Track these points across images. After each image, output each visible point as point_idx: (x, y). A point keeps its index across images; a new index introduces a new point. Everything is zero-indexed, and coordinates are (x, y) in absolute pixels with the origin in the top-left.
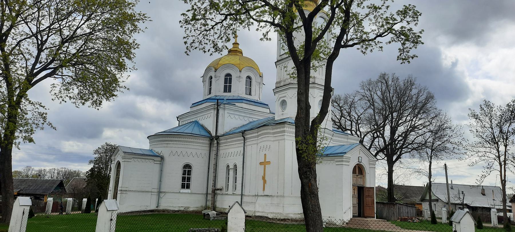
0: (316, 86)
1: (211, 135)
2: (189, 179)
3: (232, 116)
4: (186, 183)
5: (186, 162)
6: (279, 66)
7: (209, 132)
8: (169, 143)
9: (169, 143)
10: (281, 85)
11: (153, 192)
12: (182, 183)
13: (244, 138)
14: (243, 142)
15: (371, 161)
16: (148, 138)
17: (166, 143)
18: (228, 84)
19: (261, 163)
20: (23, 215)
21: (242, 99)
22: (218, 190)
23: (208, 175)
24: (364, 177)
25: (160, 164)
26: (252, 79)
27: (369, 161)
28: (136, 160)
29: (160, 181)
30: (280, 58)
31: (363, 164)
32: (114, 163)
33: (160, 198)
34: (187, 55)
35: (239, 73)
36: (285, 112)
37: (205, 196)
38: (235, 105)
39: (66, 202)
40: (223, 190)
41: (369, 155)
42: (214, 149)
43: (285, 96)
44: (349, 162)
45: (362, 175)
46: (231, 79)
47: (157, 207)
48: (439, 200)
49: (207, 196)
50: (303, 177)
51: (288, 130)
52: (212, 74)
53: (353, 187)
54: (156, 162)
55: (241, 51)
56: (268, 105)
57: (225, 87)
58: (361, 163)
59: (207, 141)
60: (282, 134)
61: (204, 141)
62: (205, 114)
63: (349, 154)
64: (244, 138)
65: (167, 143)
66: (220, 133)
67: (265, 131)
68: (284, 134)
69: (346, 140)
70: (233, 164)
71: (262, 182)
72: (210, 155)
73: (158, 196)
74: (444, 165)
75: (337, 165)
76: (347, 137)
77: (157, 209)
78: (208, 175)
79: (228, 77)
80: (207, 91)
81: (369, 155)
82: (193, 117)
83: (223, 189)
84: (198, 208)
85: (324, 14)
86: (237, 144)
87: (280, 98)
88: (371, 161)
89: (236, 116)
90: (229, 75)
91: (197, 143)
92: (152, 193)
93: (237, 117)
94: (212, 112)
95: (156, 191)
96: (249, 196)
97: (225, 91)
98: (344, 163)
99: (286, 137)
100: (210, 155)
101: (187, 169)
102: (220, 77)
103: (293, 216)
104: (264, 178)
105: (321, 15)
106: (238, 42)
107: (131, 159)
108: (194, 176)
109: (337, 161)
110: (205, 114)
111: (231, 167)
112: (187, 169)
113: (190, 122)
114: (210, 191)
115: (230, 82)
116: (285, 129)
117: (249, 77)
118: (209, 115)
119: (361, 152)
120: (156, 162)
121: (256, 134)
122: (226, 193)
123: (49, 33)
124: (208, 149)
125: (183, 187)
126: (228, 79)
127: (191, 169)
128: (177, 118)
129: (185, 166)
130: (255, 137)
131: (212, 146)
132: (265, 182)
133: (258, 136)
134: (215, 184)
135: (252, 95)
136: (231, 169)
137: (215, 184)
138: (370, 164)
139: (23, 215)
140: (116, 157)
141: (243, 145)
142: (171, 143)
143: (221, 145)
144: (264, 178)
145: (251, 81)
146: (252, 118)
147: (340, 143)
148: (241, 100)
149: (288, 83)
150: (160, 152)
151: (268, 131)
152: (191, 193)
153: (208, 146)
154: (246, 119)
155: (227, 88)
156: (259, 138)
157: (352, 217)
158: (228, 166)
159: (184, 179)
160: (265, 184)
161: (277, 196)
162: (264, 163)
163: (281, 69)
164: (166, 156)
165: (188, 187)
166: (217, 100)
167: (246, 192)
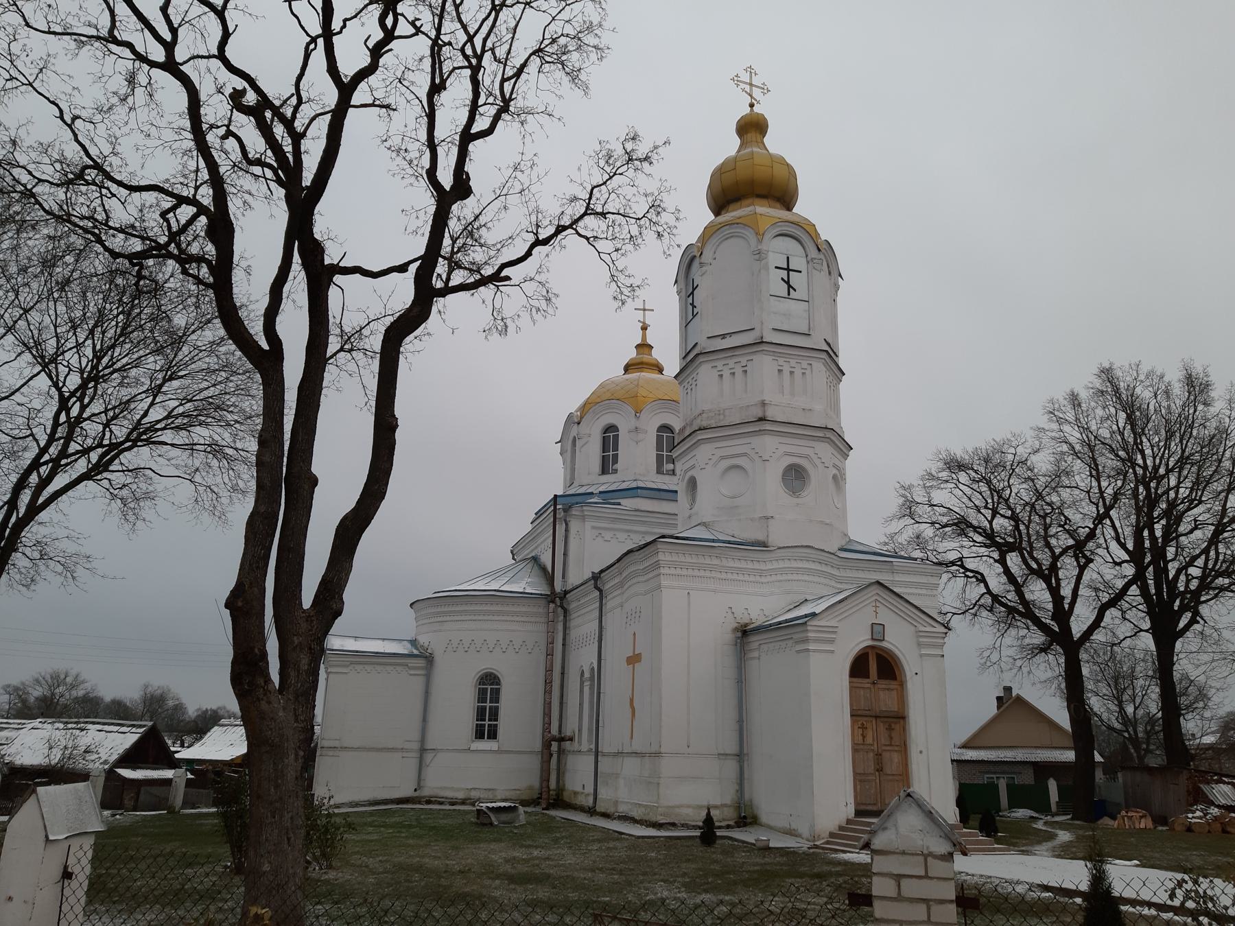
0: (768, 426)
2: (494, 714)
3: (608, 535)
4: (486, 726)
5: (484, 667)
11: (407, 751)
15: (921, 634)
24: (902, 684)
28: (359, 667)
31: (891, 643)
41: (914, 616)
43: (693, 467)
44: (832, 641)
45: (867, 680)
46: (616, 438)
47: (415, 790)
53: (854, 718)
54: (412, 672)
58: (884, 642)
63: (829, 617)
64: (601, 591)
68: (655, 573)
75: (798, 652)
76: (888, 567)
77: (417, 794)
81: (914, 616)
84: (518, 792)
85: (787, 224)
88: (921, 634)
89: (619, 535)
90: (611, 429)
101: (489, 685)
102: (590, 435)
105: (780, 229)
106: (649, 341)
108: (506, 705)
112: (489, 685)
116: (661, 556)
123: (1083, 427)
125: (479, 734)
126: (610, 437)
129: (482, 679)
138: (919, 645)
142: (448, 618)
143: (574, 616)
152: (499, 752)
158: (583, 671)
159: (481, 714)
165: (493, 735)
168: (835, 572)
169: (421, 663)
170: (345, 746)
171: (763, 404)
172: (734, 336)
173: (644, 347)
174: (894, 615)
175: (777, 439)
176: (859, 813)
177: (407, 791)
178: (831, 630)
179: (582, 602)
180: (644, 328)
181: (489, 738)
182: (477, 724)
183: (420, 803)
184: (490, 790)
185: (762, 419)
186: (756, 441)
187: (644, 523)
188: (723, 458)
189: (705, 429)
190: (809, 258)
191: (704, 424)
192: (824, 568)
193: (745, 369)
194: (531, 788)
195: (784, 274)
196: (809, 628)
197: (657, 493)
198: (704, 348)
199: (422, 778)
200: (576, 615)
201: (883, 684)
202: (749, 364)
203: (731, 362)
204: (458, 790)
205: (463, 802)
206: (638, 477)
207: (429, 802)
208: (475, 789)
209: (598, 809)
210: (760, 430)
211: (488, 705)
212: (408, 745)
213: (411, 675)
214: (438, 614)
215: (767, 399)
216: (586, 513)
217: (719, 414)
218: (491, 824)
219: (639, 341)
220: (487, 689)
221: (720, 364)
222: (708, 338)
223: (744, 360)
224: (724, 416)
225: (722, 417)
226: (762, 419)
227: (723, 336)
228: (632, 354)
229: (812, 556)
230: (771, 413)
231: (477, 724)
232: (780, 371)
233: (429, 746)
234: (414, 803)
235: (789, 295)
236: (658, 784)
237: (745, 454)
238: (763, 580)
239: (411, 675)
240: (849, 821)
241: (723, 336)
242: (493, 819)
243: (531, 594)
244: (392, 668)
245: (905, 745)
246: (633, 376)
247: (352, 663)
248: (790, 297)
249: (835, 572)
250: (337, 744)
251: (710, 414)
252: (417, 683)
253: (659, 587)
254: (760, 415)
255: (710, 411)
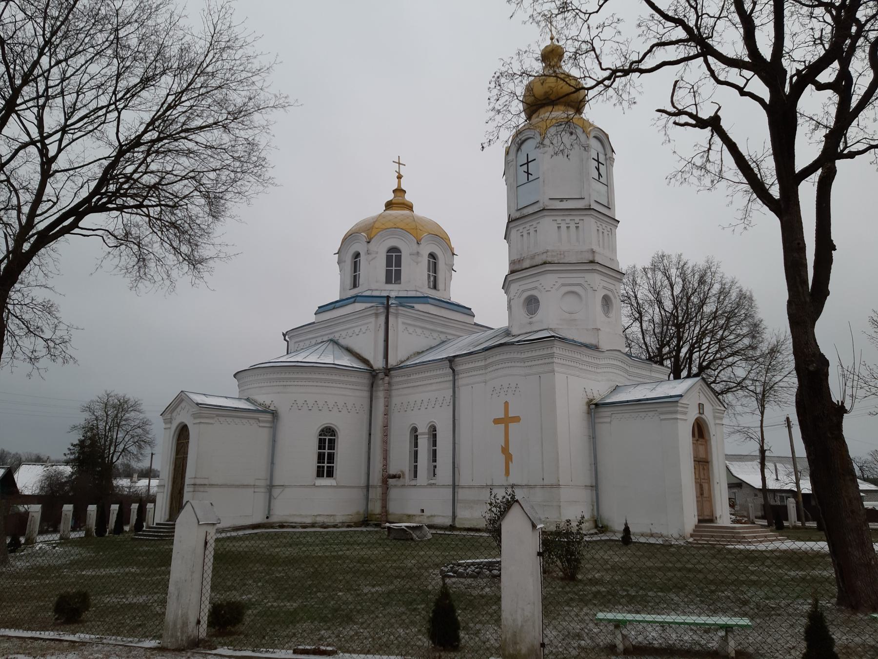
1: (372, 367)
2: (331, 458)
3: (411, 329)
5: (325, 423)
6: (518, 229)
7: (365, 361)
8: (288, 383)
9: (288, 383)
10: (524, 267)
11: (258, 487)
12: (318, 467)
13: (454, 371)
14: (451, 378)
16: (235, 376)
17: (282, 383)
18: (394, 268)
19: (497, 421)
20: (205, 549)
21: (427, 297)
22: (394, 477)
23: (369, 448)
25: (271, 427)
26: (438, 258)
27: (714, 412)
28: (222, 419)
29: (272, 463)
30: (518, 215)
32: (170, 428)
33: (272, 497)
34: (552, 156)
35: (415, 246)
36: (537, 317)
37: (451, 490)
38: (413, 307)
39: (27, 513)
40: (404, 477)
42: (380, 395)
46: (399, 259)
47: (267, 518)
48: (744, 485)
49: (368, 491)
50: (829, 435)
51: (558, 352)
52: (360, 247)
55: (411, 205)
56: (470, 309)
57: (388, 273)
59: (365, 380)
60: (547, 361)
61: (353, 379)
62: (354, 325)
64: (454, 371)
65: (285, 383)
66: (392, 362)
67: (508, 356)
68: (550, 360)
69: (648, 373)
70: (428, 424)
71: (502, 458)
72: (371, 407)
73: (268, 494)
74: (785, 419)
76: (649, 367)
77: (266, 521)
78: (369, 448)
79: (394, 254)
80: (349, 281)
82: (324, 333)
83: (404, 474)
86: (434, 383)
87: (524, 291)
91: (474, 369)
92: (256, 490)
93: (419, 331)
94: (371, 322)
95: (262, 483)
96: (470, 487)
97: (388, 281)
98: (679, 416)
99: (556, 369)
100: (371, 407)
102: (377, 253)
103: (325, 520)
104: (505, 450)
106: (403, 187)
107: (213, 418)
109: (662, 413)
110: (354, 325)
111: (423, 429)
113: (322, 342)
114: (376, 478)
115: (399, 263)
116: (554, 350)
117: (432, 256)
118: (364, 328)
119: (701, 394)
120: (261, 424)
121: (483, 363)
122: (413, 483)
124: (366, 394)
125: (320, 474)
126: (394, 257)
127: (335, 436)
128: (284, 335)
129: (322, 430)
130: (480, 368)
131: (374, 389)
132: (508, 458)
133: (486, 367)
134: (385, 466)
135: (439, 290)
136: (423, 434)
137: (385, 466)
139: (205, 549)
140: (174, 414)
141: (451, 385)
142: (292, 383)
144: (505, 450)
145: (435, 263)
146: (445, 333)
147: (641, 380)
148: (424, 299)
149: (541, 262)
150: (268, 403)
151: (512, 356)
153: (366, 388)
154: (435, 335)
155: (393, 275)
156: (489, 370)
157: (697, 523)
158: (415, 430)
159: (321, 457)
160: (510, 463)
161: (543, 486)
162: (506, 420)
163: (522, 236)
164: (283, 411)
165: (330, 474)
166: (386, 299)
167: (464, 479)
168: (627, 368)
169: (268, 417)
170: (213, 483)
171: (593, 252)
172: (569, 201)
173: (399, 191)
174: (707, 400)
175: (555, 276)
176: (700, 521)
177: (259, 518)
178: (685, 406)
179: (412, 377)
180: (400, 177)
181: (327, 477)
182: (333, 463)
183: (272, 527)
184: (331, 515)
185: (592, 262)
186: (589, 277)
187: (432, 323)
188: (564, 285)
189: (550, 263)
190: (608, 156)
191: (549, 259)
192: (623, 365)
193: (577, 225)
194: (358, 513)
195: (596, 163)
196: (679, 405)
197: (438, 302)
198: (547, 206)
199: (272, 508)
200: (397, 387)
201: (701, 440)
202: (581, 222)
203: (568, 219)
204: (306, 516)
205: (313, 525)
206: (418, 289)
207: (282, 526)
208: (320, 515)
209: (457, 525)
210: (592, 269)
211: (326, 451)
212: (258, 483)
213: (662, 420)
214: (280, 380)
215: (595, 248)
216: (400, 312)
217: (561, 254)
218: (412, 539)
219: (396, 187)
220: (326, 439)
221: (559, 219)
222: (550, 199)
223: (577, 219)
224: (564, 256)
225: (562, 256)
226: (592, 262)
227: (562, 200)
228: (390, 196)
229: (619, 357)
230: (598, 259)
231: (333, 463)
232: (559, 227)
233: (276, 483)
234: (268, 528)
235: (528, 180)
236: (560, 506)
237: (536, 288)
238: (599, 371)
239: (662, 420)
240: (696, 526)
241: (562, 200)
242: (414, 536)
243: (360, 368)
244: (246, 420)
245: (709, 478)
246: (394, 213)
247: (218, 415)
248: (530, 180)
249: (627, 368)
250: (206, 482)
251: (554, 254)
252: (264, 434)
253: (553, 371)
254: (591, 259)
255: (553, 251)
